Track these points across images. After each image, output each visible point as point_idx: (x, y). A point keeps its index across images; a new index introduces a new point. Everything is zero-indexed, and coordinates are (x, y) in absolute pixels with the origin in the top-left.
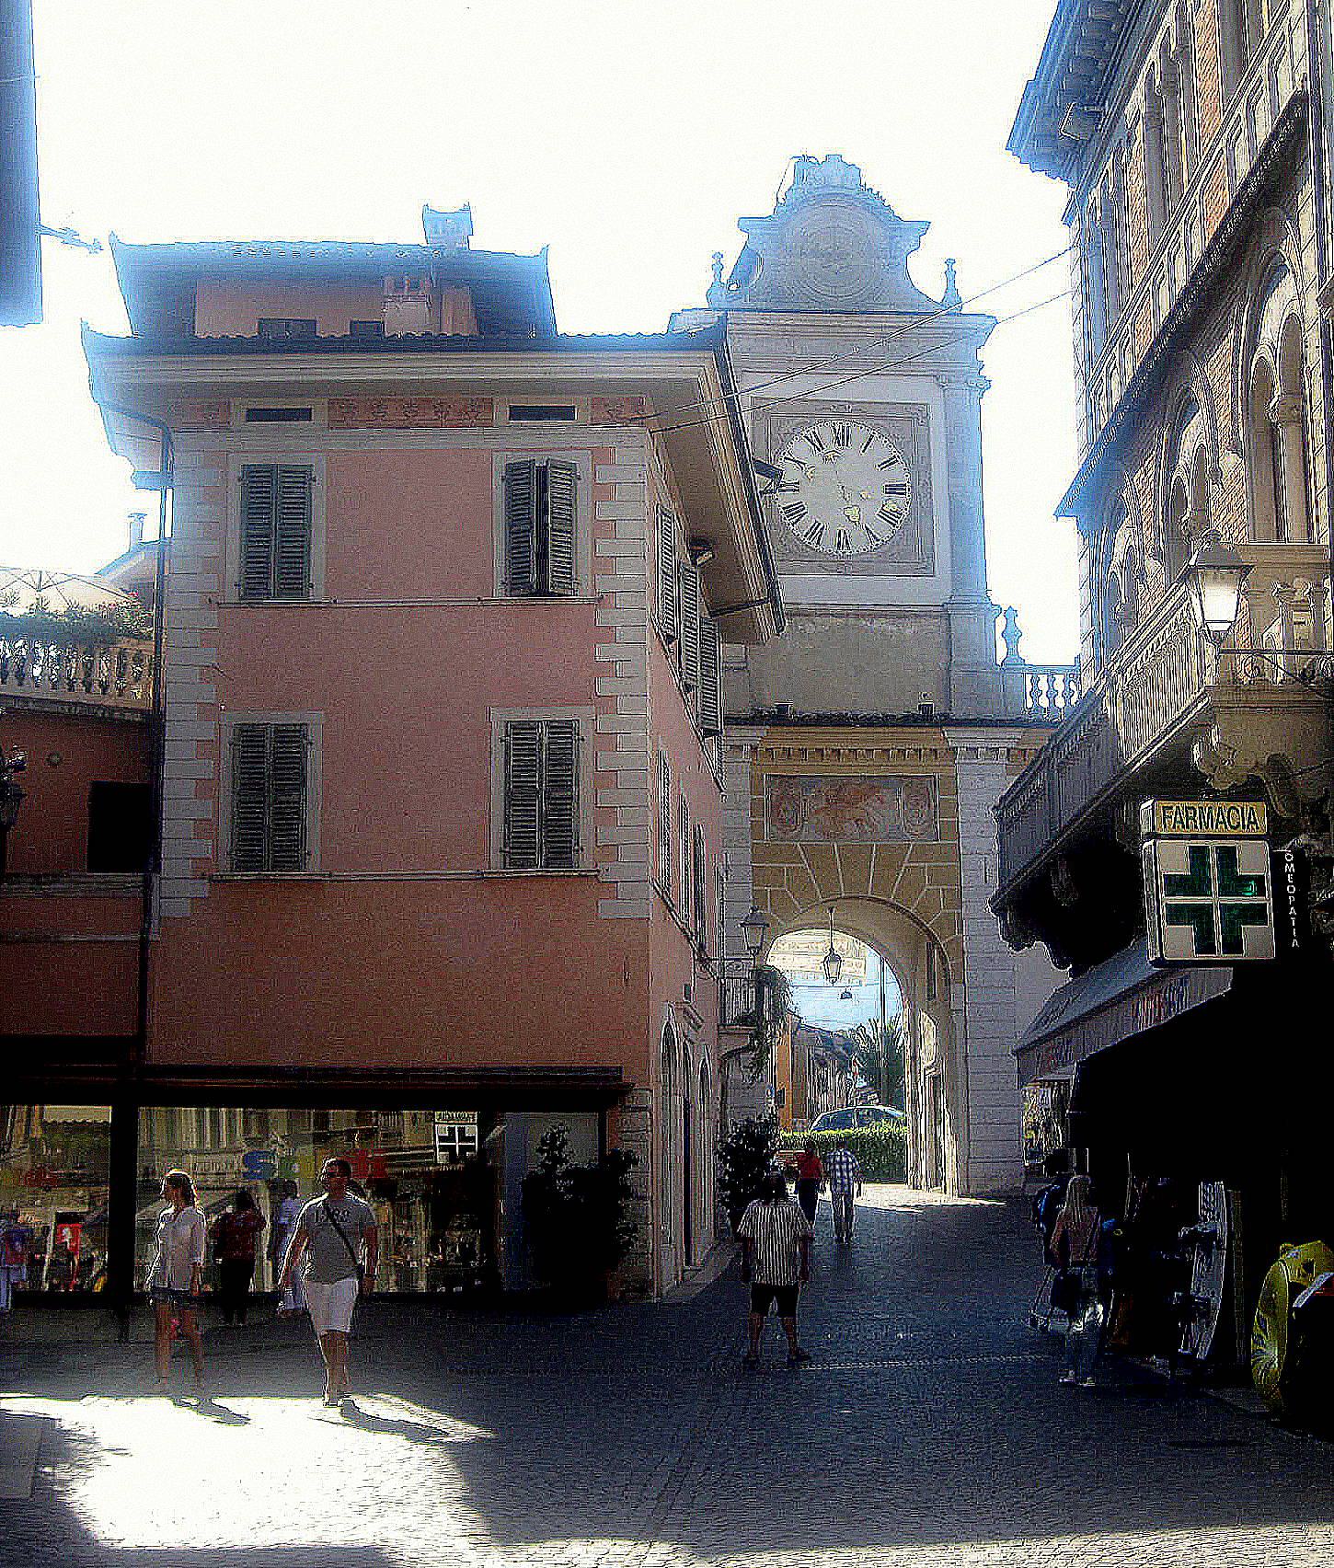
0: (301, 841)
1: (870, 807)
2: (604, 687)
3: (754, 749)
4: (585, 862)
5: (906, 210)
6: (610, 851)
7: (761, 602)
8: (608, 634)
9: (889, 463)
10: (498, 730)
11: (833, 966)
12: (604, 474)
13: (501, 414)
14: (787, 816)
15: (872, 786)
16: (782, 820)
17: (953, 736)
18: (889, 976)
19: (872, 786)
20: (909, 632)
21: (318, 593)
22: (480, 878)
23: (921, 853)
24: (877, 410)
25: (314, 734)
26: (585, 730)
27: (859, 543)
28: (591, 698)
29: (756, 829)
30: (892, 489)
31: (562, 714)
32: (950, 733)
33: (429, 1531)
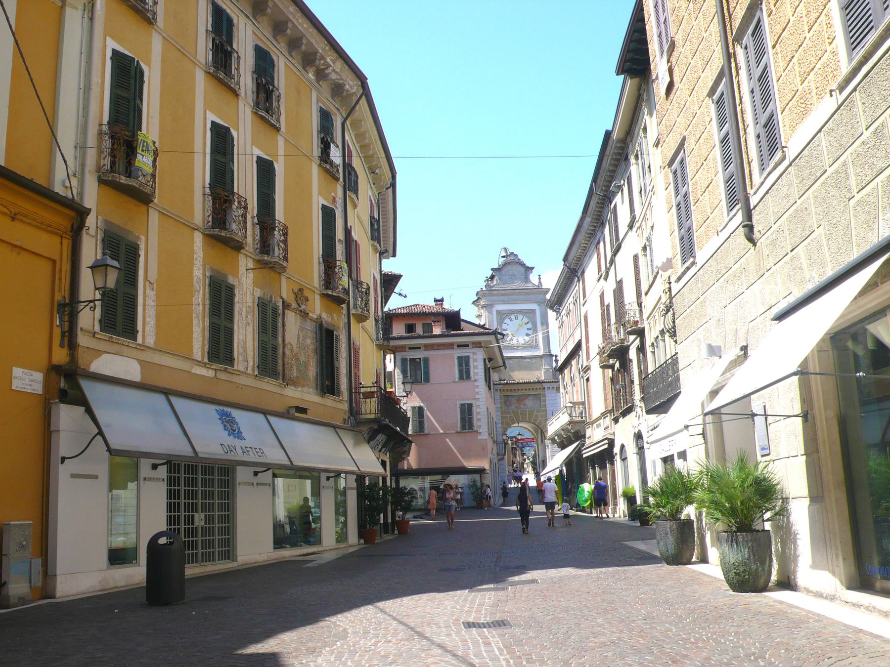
0: (424, 427)
1: (526, 402)
2: (477, 396)
4: (475, 429)
5: (529, 264)
6: (479, 427)
8: (477, 387)
9: (528, 323)
10: (458, 406)
12: (475, 357)
13: (455, 347)
15: (527, 396)
17: (545, 385)
19: (527, 396)
22: (457, 432)
23: (538, 411)
26: (474, 405)
27: (513, 317)
28: (475, 399)
29: (501, 407)
30: (528, 329)
32: (543, 384)
33: (151, 301)
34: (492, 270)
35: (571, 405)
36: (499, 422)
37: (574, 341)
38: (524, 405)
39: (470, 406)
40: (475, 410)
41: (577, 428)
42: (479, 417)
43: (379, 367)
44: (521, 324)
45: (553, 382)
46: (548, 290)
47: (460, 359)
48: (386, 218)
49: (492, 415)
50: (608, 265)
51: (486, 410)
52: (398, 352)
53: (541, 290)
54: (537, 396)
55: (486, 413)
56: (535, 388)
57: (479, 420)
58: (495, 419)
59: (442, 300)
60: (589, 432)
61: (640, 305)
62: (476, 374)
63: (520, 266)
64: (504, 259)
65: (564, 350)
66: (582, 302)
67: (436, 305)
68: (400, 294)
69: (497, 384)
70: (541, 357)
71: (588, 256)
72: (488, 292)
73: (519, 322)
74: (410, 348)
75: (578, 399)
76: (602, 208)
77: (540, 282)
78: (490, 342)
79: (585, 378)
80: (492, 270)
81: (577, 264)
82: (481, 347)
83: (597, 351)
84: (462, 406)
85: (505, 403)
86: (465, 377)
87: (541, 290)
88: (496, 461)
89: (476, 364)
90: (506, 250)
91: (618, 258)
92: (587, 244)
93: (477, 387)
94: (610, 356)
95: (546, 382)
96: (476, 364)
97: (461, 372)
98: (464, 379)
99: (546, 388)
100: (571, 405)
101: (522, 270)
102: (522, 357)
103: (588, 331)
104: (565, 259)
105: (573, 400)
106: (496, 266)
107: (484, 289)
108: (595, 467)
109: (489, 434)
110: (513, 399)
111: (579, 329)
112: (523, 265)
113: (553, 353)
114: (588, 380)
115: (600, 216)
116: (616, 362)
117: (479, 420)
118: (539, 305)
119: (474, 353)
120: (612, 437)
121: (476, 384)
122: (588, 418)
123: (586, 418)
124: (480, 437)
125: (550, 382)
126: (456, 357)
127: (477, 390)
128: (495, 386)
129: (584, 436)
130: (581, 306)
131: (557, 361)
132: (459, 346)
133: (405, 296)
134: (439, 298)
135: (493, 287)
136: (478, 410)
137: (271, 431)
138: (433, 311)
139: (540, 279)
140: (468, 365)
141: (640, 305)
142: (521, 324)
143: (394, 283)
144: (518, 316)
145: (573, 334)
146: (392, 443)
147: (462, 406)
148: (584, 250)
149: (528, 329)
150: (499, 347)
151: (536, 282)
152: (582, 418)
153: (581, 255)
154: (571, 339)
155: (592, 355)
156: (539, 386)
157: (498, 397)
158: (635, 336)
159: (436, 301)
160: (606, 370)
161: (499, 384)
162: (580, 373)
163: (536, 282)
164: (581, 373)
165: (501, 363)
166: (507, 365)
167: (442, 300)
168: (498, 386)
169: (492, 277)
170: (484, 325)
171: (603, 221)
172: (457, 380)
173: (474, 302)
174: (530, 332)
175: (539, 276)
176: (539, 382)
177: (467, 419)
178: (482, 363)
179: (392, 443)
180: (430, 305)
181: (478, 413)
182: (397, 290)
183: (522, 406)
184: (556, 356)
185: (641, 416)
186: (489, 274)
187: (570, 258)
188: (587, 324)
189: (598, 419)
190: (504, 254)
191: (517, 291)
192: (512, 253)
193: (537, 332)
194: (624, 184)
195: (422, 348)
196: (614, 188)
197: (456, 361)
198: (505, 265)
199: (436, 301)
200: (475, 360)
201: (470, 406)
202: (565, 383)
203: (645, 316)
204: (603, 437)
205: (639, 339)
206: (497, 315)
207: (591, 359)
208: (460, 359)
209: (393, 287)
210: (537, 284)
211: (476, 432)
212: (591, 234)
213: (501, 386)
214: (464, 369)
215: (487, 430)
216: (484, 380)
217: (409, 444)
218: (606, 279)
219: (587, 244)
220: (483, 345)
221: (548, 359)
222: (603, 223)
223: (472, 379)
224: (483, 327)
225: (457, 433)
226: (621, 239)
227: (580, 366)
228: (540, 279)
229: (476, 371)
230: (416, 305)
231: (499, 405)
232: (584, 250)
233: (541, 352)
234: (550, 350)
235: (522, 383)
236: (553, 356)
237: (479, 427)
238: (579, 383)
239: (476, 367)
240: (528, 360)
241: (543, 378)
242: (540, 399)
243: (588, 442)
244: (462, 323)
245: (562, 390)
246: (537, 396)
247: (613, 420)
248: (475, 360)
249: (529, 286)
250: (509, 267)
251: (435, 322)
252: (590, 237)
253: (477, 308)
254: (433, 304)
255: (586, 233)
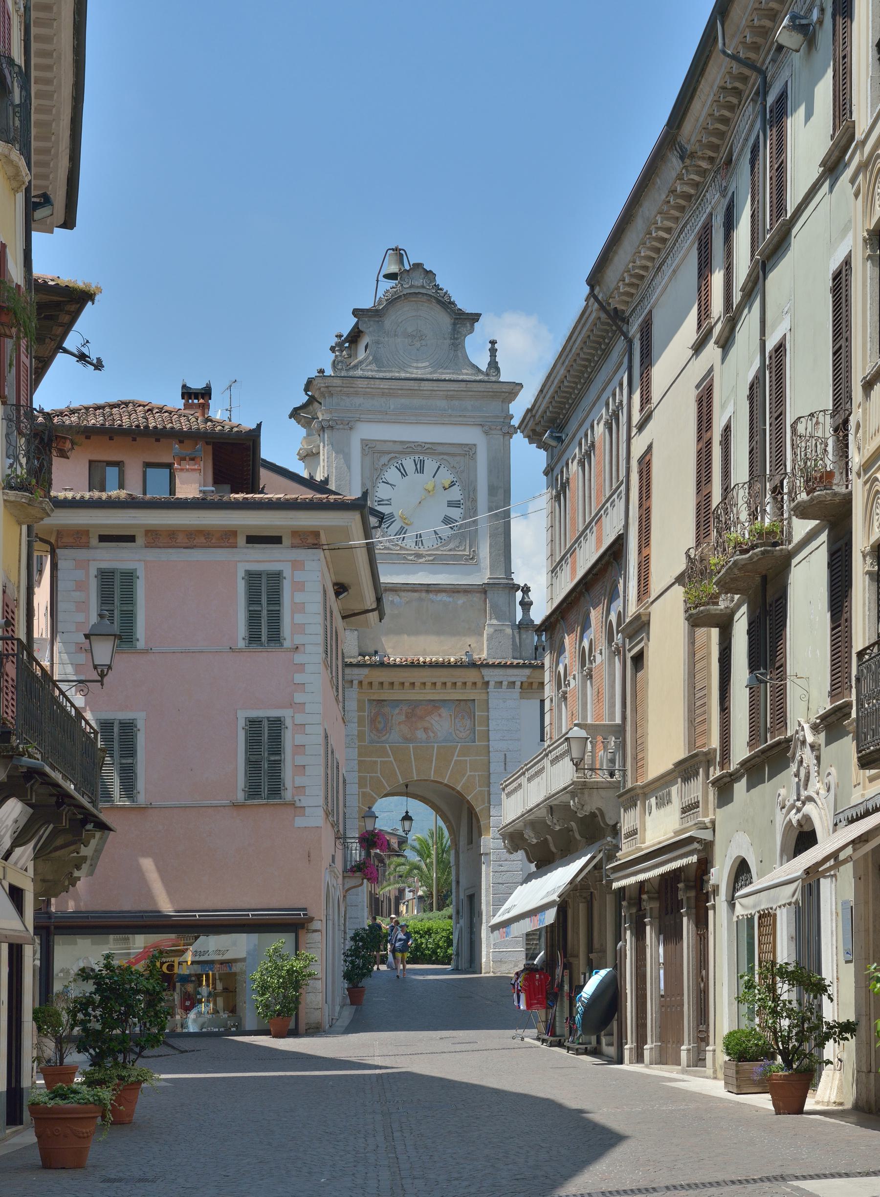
2: (299, 698)
3: (360, 683)
4: (288, 795)
5: (465, 304)
6: (301, 789)
7: (373, 610)
8: (301, 667)
9: (452, 484)
10: (241, 723)
11: (407, 823)
12: (299, 576)
13: (241, 540)
14: (380, 726)
15: (436, 705)
16: (378, 730)
18: (438, 817)
19: (436, 705)
20: (460, 602)
21: (141, 645)
24: (440, 449)
25: (140, 724)
26: (288, 722)
28: (291, 705)
29: (361, 736)
30: (451, 504)
31: (274, 713)
32: (485, 672)
34: (356, 312)
35: (583, 733)
36: (353, 778)
37: (599, 541)
38: (426, 730)
39: (277, 724)
40: (289, 739)
41: (594, 803)
42: (300, 760)
43: (14, 578)
44: (430, 486)
45: (512, 666)
46: (514, 389)
47: (253, 578)
48: (49, 82)
49: (337, 755)
50: (737, 296)
51: (321, 740)
52: (65, 547)
53: (496, 387)
54: (465, 707)
55: (322, 751)
56: (449, 681)
57: (301, 769)
58: (343, 770)
59: (206, 393)
60: (628, 820)
61: (841, 429)
62: (300, 628)
63: (438, 308)
64: (392, 283)
65: (567, 569)
66: (636, 418)
67: (187, 406)
68: (82, 357)
69: (351, 665)
70: (484, 590)
71: (668, 270)
72: (338, 382)
73: (426, 480)
74: (103, 538)
75: (599, 716)
76: (732, 108)
77: (493, 365)
78: (346, 533)
79: (629, 655)
80: (356, 312)
81: (632, 295)
82: (316, 546)
83: (681, 566)
84: (254, 724)
85: (373, 721)
86: (264, 638)
87: (496, 387)
88: (339, 893)
89: (299, 597)
90: (399, 254)
91: (773, 278)
92: (669, 230)
93: (301, 667)
94: (727, 586)
95: (493, 666)
96: (299, 597)
97: (253, 619)
98: (262, 644)
99: (492, 684)
100: (583, 733)
101: (445, 320)
102: (429, 589)
103: (648, 510)
104: (594, 279)
105: (585, 717)
106: (367, 303)
107: (329, 372)
108: (645, 925)
109: (327, 814)
110: (397, 711)
111: (621, 505)
112: (446, 304)
113: (519, 579)
114: (639, 660)
115: (721, 135)
116: (738, 606)
117: (301, 769)
118: (486, 433)
119: (297, 565)
120: (706, 835)
121: (298, 658)
122: (629, 773)
123: (624, 776)
124: (300, 822)
125: (505, 666)
126: (241, 574)
127: (298, 678)
128: (348, 671)
129: (615, 831)
130: (634, 431)
131: (526, 605)
132: (253, 540)
133: (98, 366)
134: (197, 385)
135: (356, 367)
136: (300, 739)
137: (663, 597)
138: (177, 426)
139: (493, 352)
140: (275, 598)
141: (841, 429)
142: (430, 486)
143: (66, 319)
144: (422, 462)
145: (597, 519)
146: (46, 831)
147: (254, 724)
148: (658, 250)
149: (451, 504)
150: (370, 549)
151: (482, 362)
152: (612, 775)
153: (645, 268)
154: (592, 538)
155: (658, 580)
156: (472, 675)
157: (352, 705)
158: (812, 524)
159: (188, 394)
160: (701, 632)
161: (358, 665)
162: (610, 639)
163: (482, 362)
164: (618, 638)
165: (370, 602)
166: (387, 609)
167: (206, 393)
168: (356, 671)
169: (355, 336)
170: (326, 481)
171: (731, 154)
172: (241, 644)
173: (295, 413)
174: (455, 513)
175: (493, 343)
176: (473, 665)
177: (265, 765)
178: (319, 597)
179: (46, 831)
180: (170, 407)
181: (300, 749)
182: (71, 342)
183: (420, 734)
184: (526, 590)
185: (813, 774)
186: (347, 324)
187: (612, 275)
188: (648, 485)
189: (665, 781)
190: (394, 268)
191: (426, 385)
192: (418, 266)
193: (475, 513)
194: (821, 22)
195: (140, 541)
196: (786, 33)
197: (241, 587)
198: (393, 301)
199: (188, 394)
200: (299, 587)
201: (277, 724)
202: (561, 668)
203: (856, 459)
204: (677, 833)
205: (824, 537)
206: (364, 454)
207: (653, 595)
208: (253, 578)
209: (59, 330)
210: (484, 367)
211: (292, 804)
212: (688, 197)
213: (366, 671)
214: (264, 613)
215: (321, 801)
216: (321, 649)
217: (98, 835)
218: (726, 343)
219: (669, 230)
220: (323, 540)
221: (500, 598)
222: (729, 162)
223: (287, 644)
224: (322, 487)
225: (235, 805)
226: (791, 207)
227: (613, 617)
228: (493, 352)
229: (299, 618)
230: (126, 404)
231: (354, 728)
232: (658, 250)
233: (483, 577)
234: (508, 572)
235: (425, 665)
236: (516, 587)
237: (301, 789)
238: (606, 667)
239: (299, 608)
240: (443, 597)
241: (484, 655)
242: (472, 716)
243: (627, 851)
244: (263, 473)
245: (549, 691)
246: (465, 707)
247: (714, 783)
248: (299, 587)
249: (466, 374)
250: (404, 313)
251: (183, 459)
252: (682, 209)
253: (303, 432)
254: (178, 403)
255: (673, 191)
